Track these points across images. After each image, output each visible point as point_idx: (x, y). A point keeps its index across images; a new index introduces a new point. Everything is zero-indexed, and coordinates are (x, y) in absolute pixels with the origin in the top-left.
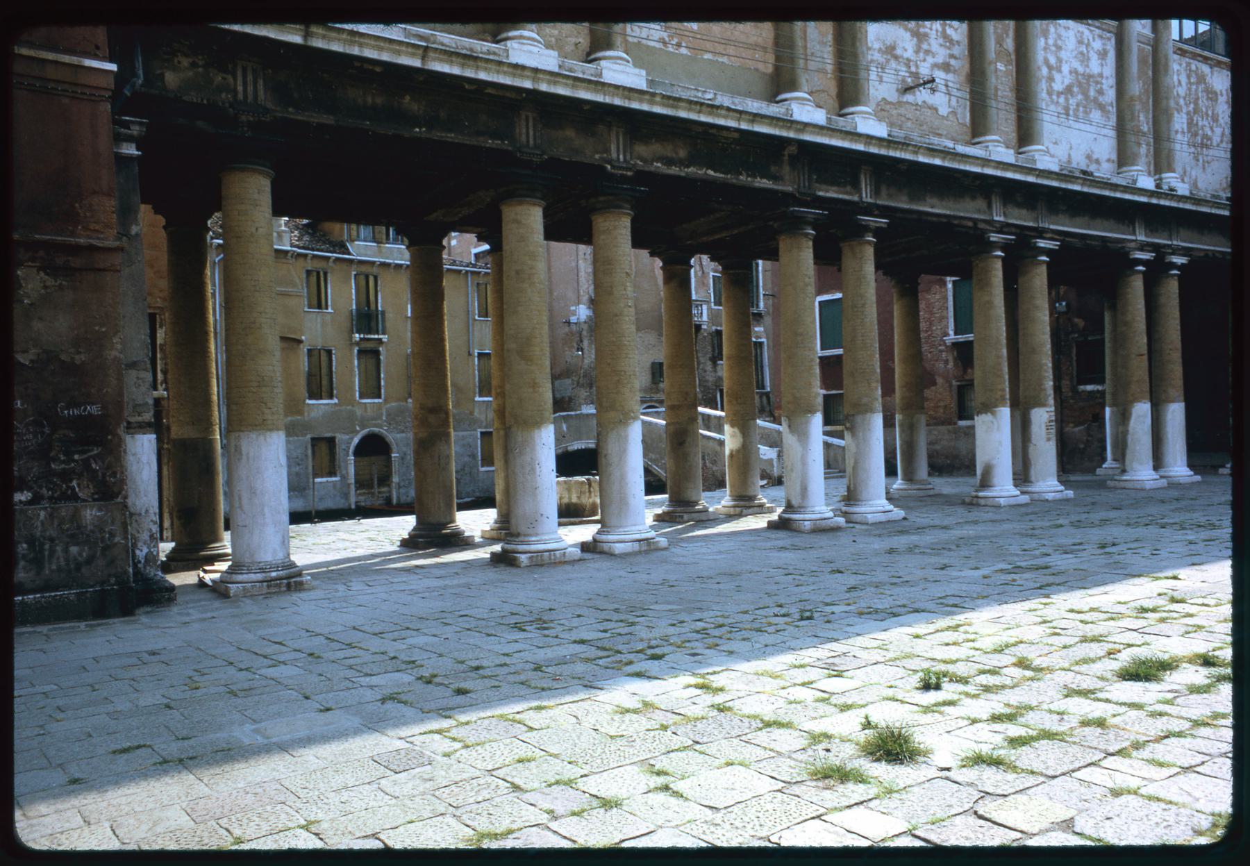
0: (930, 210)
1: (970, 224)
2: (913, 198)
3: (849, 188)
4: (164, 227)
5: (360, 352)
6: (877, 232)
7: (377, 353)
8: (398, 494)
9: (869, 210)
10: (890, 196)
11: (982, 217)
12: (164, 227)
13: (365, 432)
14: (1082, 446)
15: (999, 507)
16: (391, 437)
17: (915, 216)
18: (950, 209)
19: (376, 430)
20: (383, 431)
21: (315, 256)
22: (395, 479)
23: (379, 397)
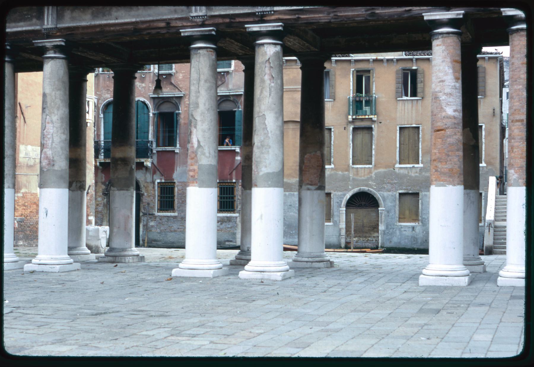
0: (117, 21)
1: (163, 25)
2: (95, 16)
3: (34, 20)
4: (244, 71)
5: (355, 129)
6: (57, 48)
7: (370, 129)
8: (382, 240)
9: (49, 34)
10: (73, 19)
11: (176, 16)
12: (244, 71)
13: (356, 190)
14: (21, 243)
15: (240, 279)
16: (378, 195)
17: (98, 30)
18: (133, 17)
19: (365, 189)
20: (373, 190)
21: (417, 59)
22: (382, 227)
23: (371, 164)
